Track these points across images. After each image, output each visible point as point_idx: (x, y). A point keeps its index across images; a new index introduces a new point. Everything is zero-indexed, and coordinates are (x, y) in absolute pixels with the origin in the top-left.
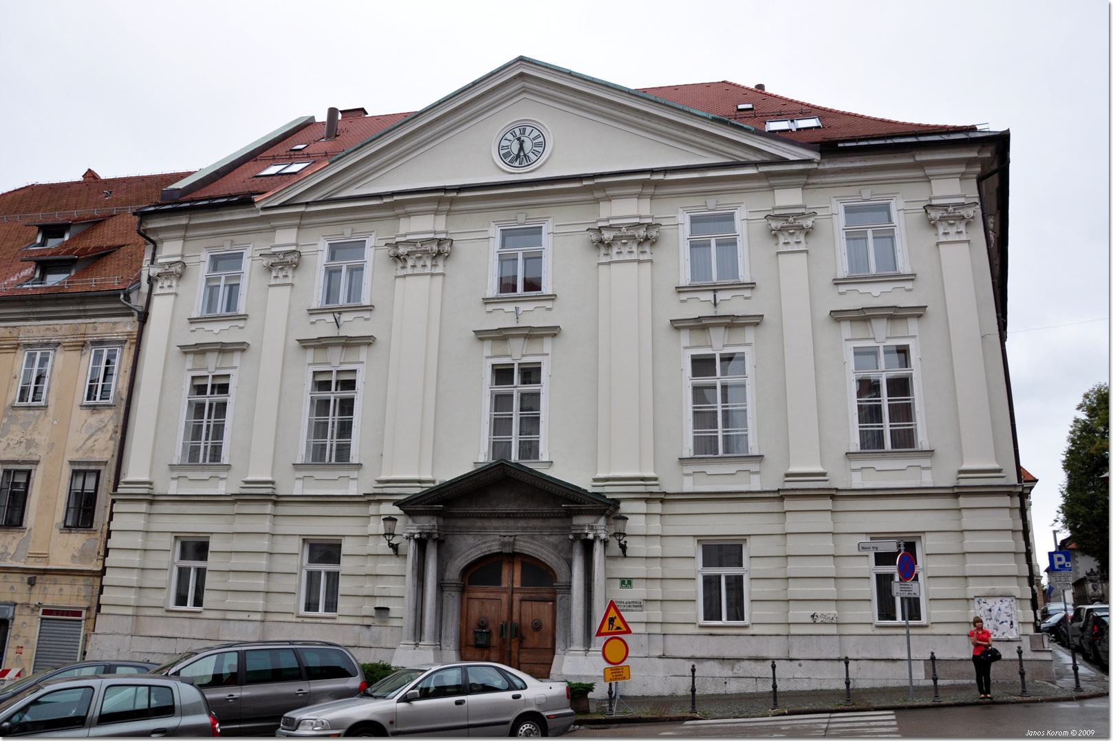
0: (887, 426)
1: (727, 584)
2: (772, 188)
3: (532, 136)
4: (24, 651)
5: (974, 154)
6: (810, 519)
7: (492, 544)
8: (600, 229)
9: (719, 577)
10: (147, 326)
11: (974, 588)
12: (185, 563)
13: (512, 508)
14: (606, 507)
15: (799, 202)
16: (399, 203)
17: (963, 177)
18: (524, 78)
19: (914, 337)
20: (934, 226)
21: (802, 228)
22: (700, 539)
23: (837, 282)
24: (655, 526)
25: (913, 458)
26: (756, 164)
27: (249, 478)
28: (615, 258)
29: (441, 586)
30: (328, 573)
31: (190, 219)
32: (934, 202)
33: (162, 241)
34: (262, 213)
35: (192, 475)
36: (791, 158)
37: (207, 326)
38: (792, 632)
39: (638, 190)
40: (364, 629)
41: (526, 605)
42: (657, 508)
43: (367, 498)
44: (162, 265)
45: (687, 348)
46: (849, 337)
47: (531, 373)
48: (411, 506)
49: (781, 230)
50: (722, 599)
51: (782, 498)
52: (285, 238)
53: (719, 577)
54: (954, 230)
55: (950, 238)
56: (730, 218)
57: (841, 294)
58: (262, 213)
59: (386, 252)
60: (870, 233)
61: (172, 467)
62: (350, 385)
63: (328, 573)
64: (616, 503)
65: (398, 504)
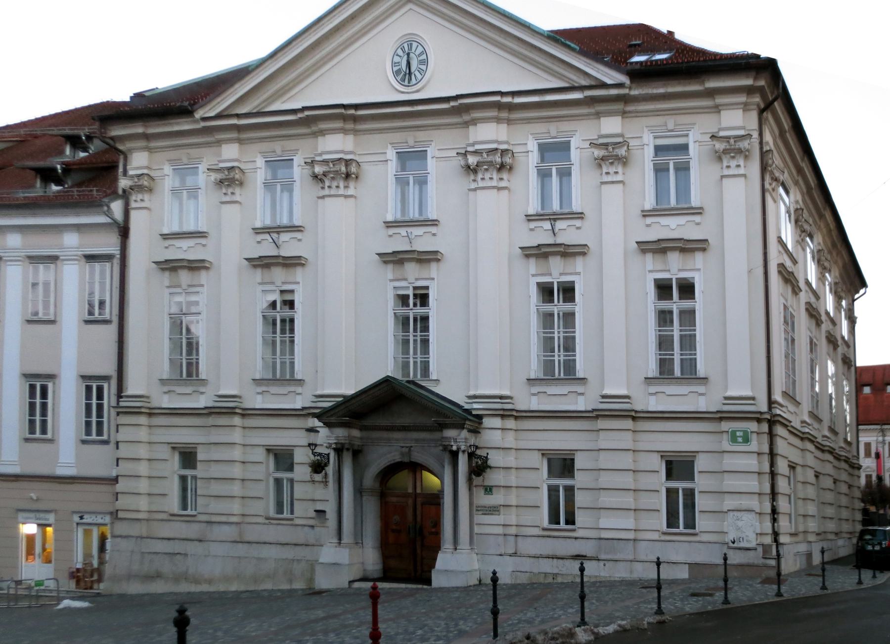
1: (684, 495)
2: (598, 115)
3: (417, 53)
5: (748, 82)
8: (465, 155)
9: (677, 490)
11: (729, 503)
14: (470, 420)
16: (313, 120)
17: (746, 107)
19: (579, 274)
20: (720, 159)
21: (740, 151)
22: (663, 455)
23: (645, 214)
24: (510, 440)
26: (582, 88)
27: (319, 392)
28: (481, 184)
29: (359, 491)
33: (131, 150)
34: (203, 124)
35: (180, 390)
36: (609, 82)
37: (664, 221)
38: (603, 536)
42: (511, 423)
43: (719, 415)
44: (132, 177)
45: (653, 269)
46: (651, 268)
52: (230, 152)
58: (203, 124)
59: (307, 171)
61: (163, 381)
64: (480, 417)
65: (318, 416)
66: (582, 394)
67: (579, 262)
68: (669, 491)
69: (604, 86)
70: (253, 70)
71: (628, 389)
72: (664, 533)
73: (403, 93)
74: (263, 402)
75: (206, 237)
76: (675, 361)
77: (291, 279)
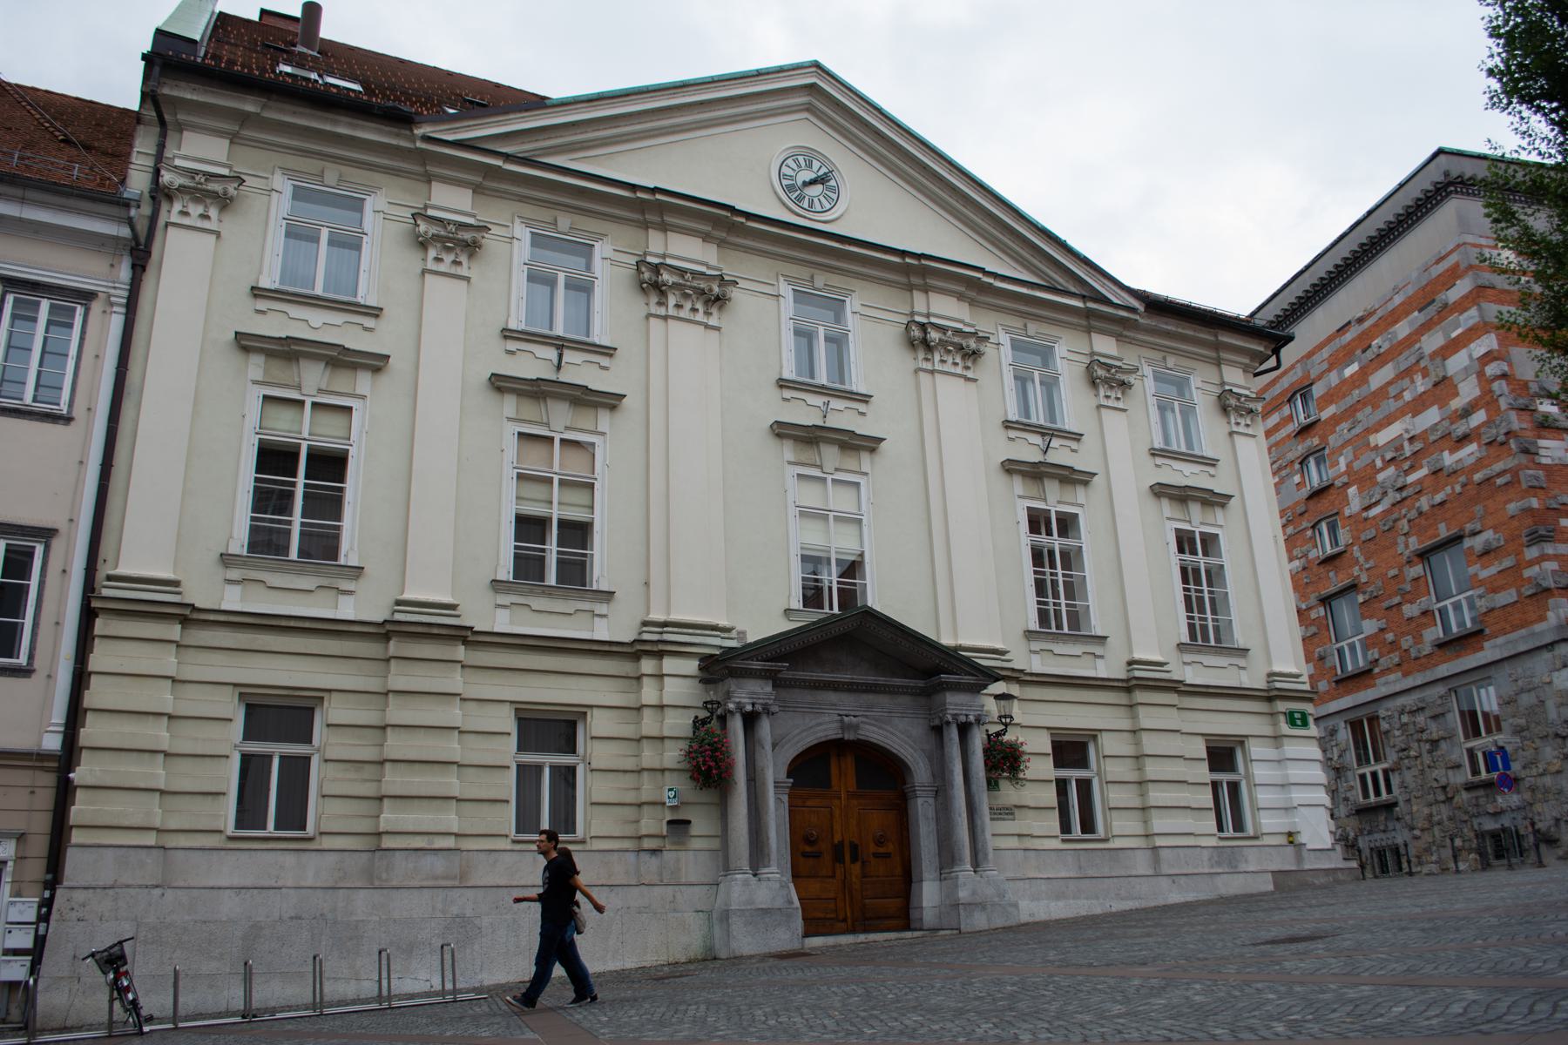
0: (552, 549)
6: (1155, 714)
7: (824, 727)
12: (530, 758)
13: (845, 677)
15: (1114, 353)
16: (653, 208)
18: (816, 94)
19: (1081, 506)
25: (1086, 643)
30: (555, 769)
31: (264, 107)
32: (430, 212)
33: (180, 128)
34: (419, 144)
36: (1116, 301)
39: (962, 289)
45: (1168, 520)
47: (1067, 524)
48: (719, 667)
49: (436, 238)
50: (272, 795)
51: (387, 637)
53: (268, 758)
54: (1242, 422)
55: (442, 268)
56: (357, 205)
57: (785, 400)
58: (419, 144)
60: (325, 234)
63: (555, 769)
66: (1101, 657)
67: (604, 420)
68: (246, 759)
69: (1108, 302)
70: (547, 107)
72: (514, 842)
74: (511, 623)
75: (611, 356)
76: (1206, 623)
77: (1211, 520)
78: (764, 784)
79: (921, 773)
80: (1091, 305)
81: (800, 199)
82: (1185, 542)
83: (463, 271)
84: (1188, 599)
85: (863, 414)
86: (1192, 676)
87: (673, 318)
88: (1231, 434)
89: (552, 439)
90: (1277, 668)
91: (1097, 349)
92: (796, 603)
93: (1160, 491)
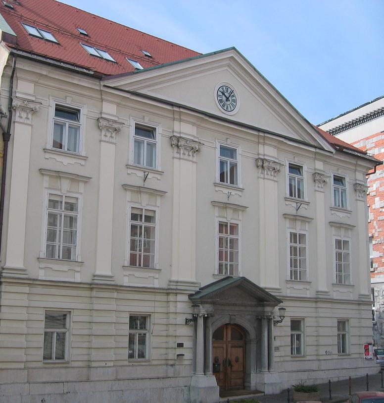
4: (69, 394)
10: (10, 143)
19: (81, 193)
26: (315, 147)
36: (326, 149)
40: (170, 367)
41: (233, 349)
45: (336, 235)
47: (234, 228)
48: (195, 299)
62: (71, 207)
68: (46, 334)
69: (323, 149)
71: (280, 286)
73: (223, 113)
76: (140, 257)
78: (264, 341)
79: (252, 334)
80: (318, 151)
81: (224, 106)
82: (294, 237)
83: (113, 140)
84: (221, 253)
85: (240, 196)
86: (335, 296)
87: (182, 159)
88: (100, 141)
89: (142, 209)
90: (320, 289)
91: (357, 178)
92: (216, 272)
93: (332, 224)
